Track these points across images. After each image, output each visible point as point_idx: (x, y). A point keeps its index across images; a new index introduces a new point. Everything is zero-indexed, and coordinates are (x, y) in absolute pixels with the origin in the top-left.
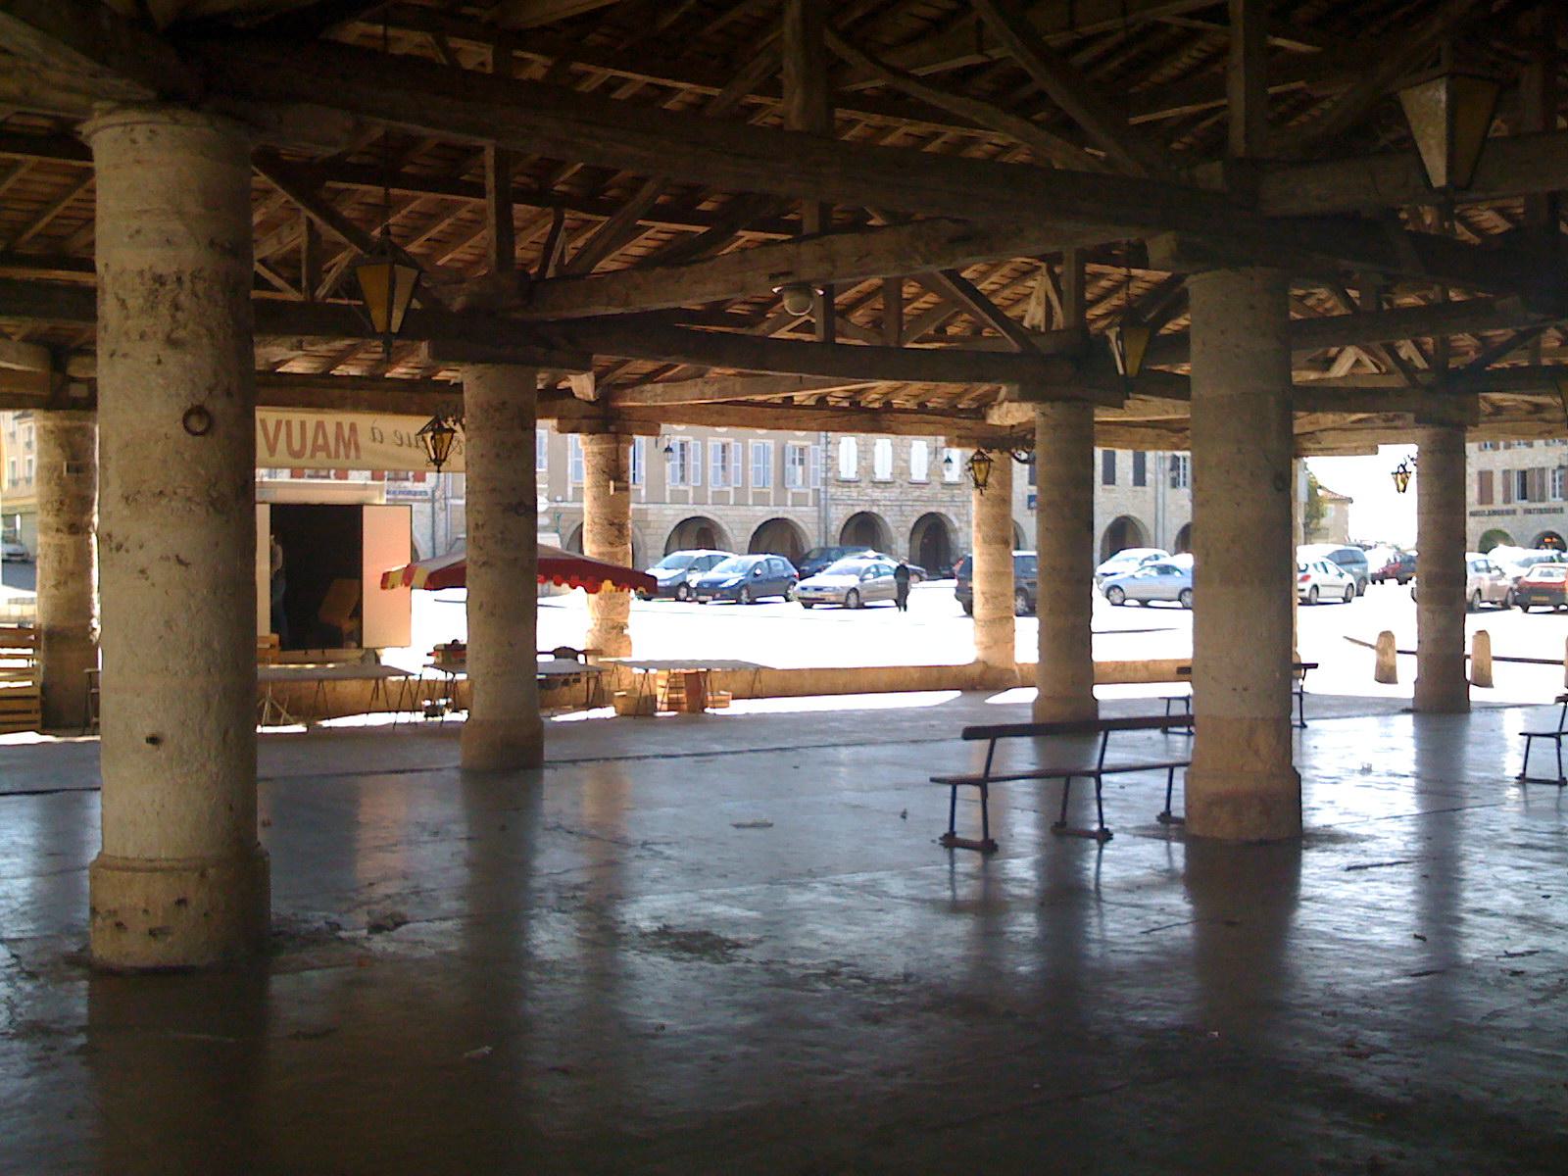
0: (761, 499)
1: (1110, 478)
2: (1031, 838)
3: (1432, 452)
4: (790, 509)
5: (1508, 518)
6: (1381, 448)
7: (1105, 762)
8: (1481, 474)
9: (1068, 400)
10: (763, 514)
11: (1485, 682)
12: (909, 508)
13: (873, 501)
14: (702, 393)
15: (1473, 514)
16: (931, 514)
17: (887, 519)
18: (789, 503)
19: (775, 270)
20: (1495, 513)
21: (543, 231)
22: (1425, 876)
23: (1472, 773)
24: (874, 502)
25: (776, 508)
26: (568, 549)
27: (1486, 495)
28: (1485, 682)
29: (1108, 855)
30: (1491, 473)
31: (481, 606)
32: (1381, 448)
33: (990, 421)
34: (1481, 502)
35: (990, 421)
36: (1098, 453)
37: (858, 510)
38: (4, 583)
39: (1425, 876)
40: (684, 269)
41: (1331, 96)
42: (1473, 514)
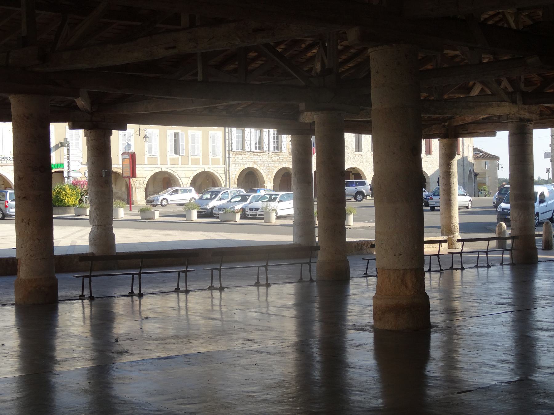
0: (196, 162)
1: (429, 152)
3: (529, 145)
4: (211, 166)
10: (197, 170)
12: (273, 165)
13: (254, 162)
17: (262, 171)
18: (210, 163)
21: (209, 366)
22: (24, 198)
24: (254, 163)
25: (204, 166)
26: (499, 207)
29: (537, 239)
30: (426, 154)
31: (23, 220)
36: (424, 142)
37: (246, 166)
38: (70, 129)
39: (24, 198)
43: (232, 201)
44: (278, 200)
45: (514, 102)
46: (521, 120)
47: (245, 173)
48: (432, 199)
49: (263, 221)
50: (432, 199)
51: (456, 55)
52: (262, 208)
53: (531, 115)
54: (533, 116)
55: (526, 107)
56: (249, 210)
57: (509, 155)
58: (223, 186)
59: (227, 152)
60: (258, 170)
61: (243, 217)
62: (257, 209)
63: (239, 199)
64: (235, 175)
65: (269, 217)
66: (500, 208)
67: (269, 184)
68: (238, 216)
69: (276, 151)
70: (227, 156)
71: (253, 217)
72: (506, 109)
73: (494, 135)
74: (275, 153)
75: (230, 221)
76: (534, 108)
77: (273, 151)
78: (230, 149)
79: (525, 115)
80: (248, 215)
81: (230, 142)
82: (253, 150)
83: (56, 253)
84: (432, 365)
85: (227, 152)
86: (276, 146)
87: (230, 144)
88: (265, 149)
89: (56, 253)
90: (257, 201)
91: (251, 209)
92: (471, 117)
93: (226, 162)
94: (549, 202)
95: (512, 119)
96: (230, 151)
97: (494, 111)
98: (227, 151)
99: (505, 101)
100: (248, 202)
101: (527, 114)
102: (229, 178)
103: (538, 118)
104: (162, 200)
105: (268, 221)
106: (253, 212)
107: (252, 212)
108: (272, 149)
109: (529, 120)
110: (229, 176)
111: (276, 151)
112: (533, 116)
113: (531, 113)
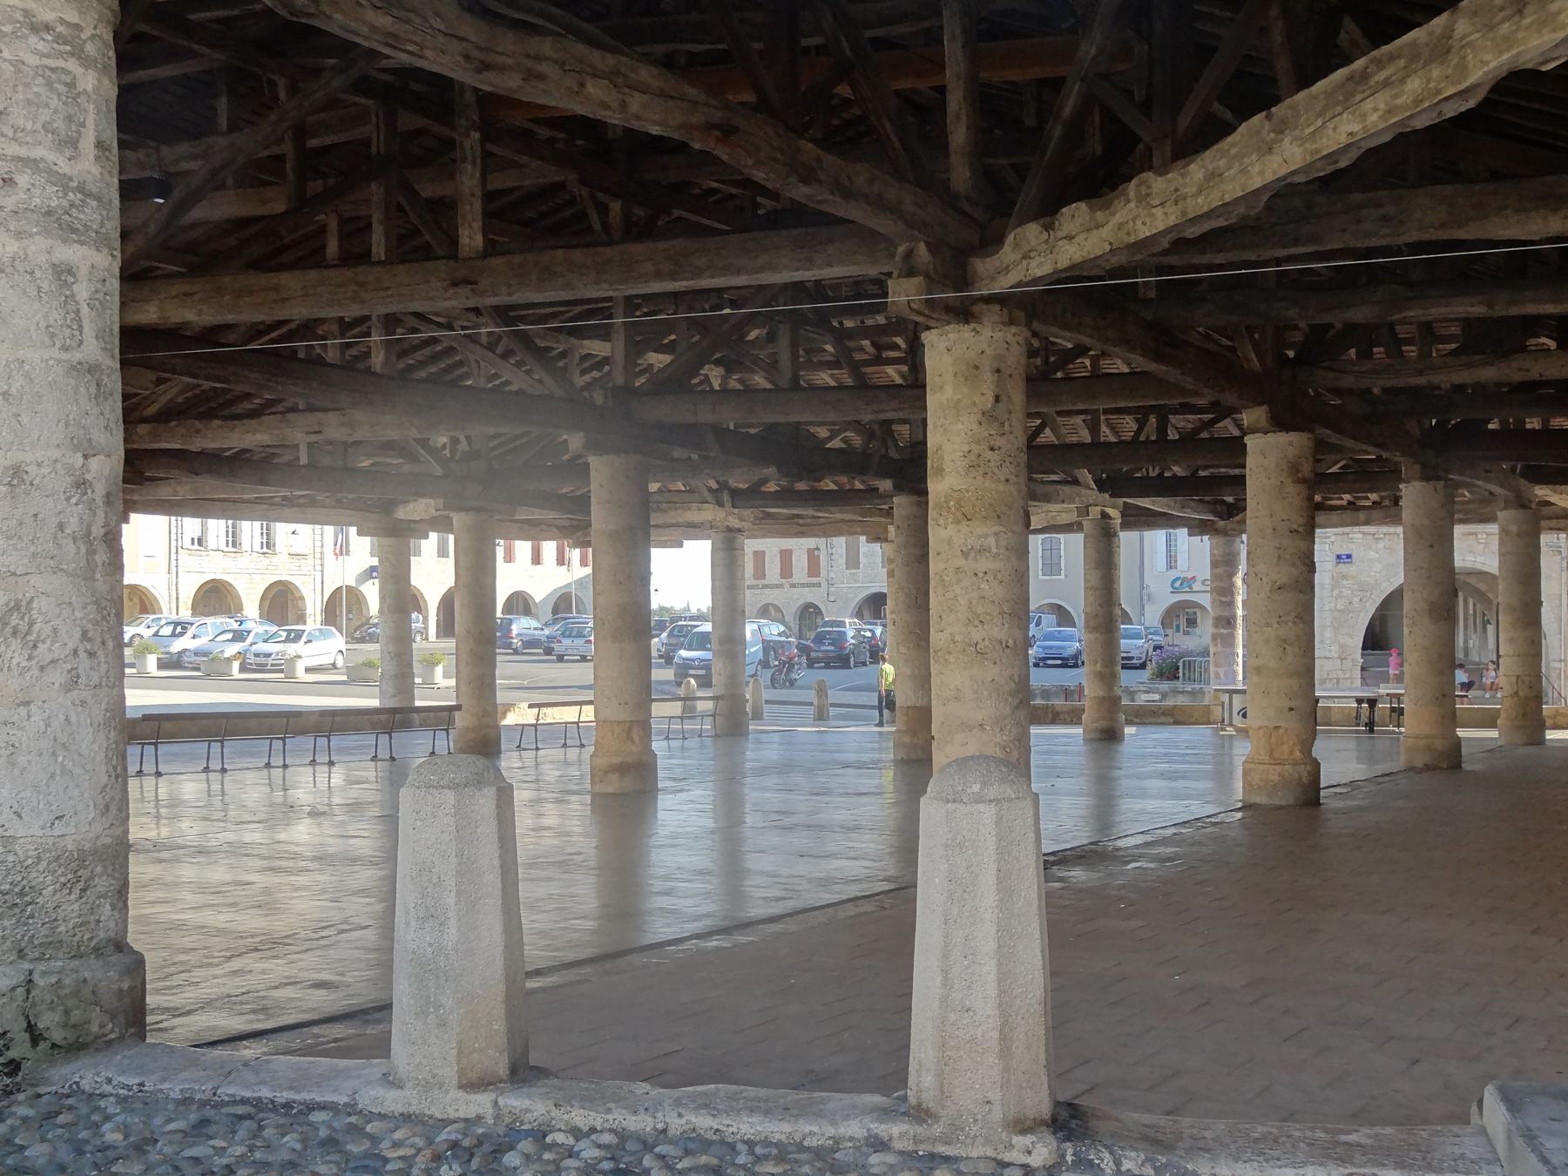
2: (1122, 801)
5: (777, 591)
6: (686, 543)
7: (530, 921)
8: (755, 553)
9: (478, 510)
11: (757, 715)
14: (176, 491)
15: (750, 587)
16: (279, 583)
19: (310, 429)
20: (766, 587)
23: (1138, 805)
27: (760, 572)
28: (757, 715)
32: (686, 543)
33: (396, 516)
34: (756, 577)
35: (396, 516)
40: (235, 422)
41: (956, 1159)
42: (750, 587)
43: (216, 639)
44: (304, 639)
45: (720, 504)
46: (729, 529)
47: (276, 589)
48: (559, 641)
49: (282, 675)
50: (559, 641)
51: (279, 321)
52: (277, 654)
53: (743, 523)
54: (745, 525)
55: (736, 511)
56: (253, 657)
57: (713, 580)
58: (165, 610)
59: (174, 550)
60: (231, 585)
61: (243, 669)
62: (269, 655)
63: (229, 636)
64: (188, 595)
65: (293, 670)
66: (680, 657)
67: (251, 608)
68: (236, 665)
69: (265, 550)
70: (173, 556)
71: (261, 668)
72: (709, 513)
73: (681, 546)
74: (264, 553)
75: (222, 674)
76: (747, 513)
77: (806, 580)
78: (180, 545)
79: (734, 522)
80: (251, 664)
81: (180, 531)
82: (223, 546)
83: (129, 715)
84: (966, 727)
85: (174, 550)
86: (265, 541)
87: (180, 536)
88: (246, 545)
89: (129, 715)
90: (266, 641)
91: (257, 655)
92: (964, 562)
93: (173, 567)
94: (752, 650)
95: (717, 528)
96: (180, 549)
97: (693, 516)
98: (174, 550)
99: (707, 503)
100: (248, 642)
101: (736, 521)
102: (177, 598)
103: (751, 526)
104: (133, 636)
105: (291, 675)
106: (262, 660)
107: (258, 660)
108: (257, 547)
109: (739, 530)
110: (177, 594)
111: (265, 550)
112: (745, 525)
113: (742, 519)
